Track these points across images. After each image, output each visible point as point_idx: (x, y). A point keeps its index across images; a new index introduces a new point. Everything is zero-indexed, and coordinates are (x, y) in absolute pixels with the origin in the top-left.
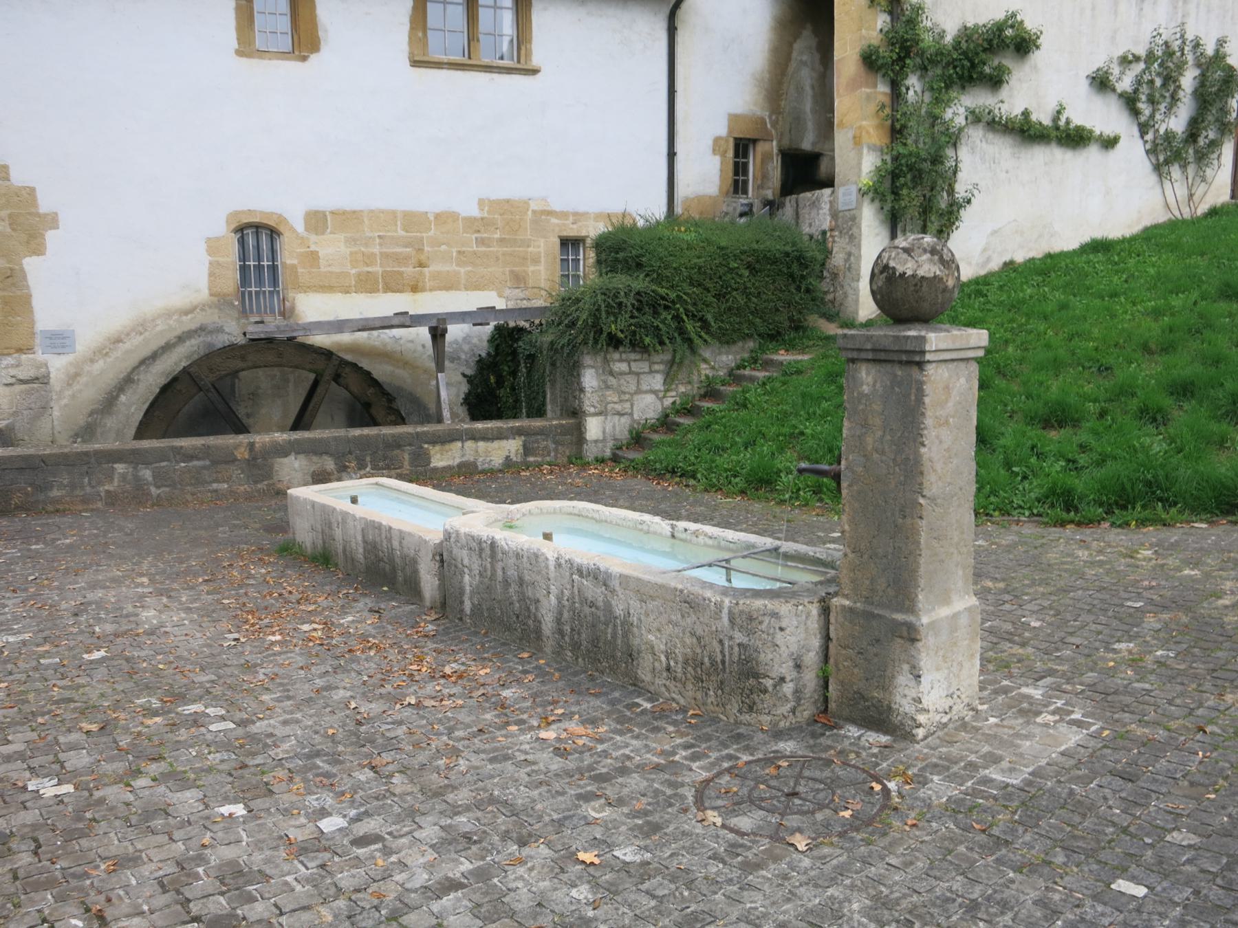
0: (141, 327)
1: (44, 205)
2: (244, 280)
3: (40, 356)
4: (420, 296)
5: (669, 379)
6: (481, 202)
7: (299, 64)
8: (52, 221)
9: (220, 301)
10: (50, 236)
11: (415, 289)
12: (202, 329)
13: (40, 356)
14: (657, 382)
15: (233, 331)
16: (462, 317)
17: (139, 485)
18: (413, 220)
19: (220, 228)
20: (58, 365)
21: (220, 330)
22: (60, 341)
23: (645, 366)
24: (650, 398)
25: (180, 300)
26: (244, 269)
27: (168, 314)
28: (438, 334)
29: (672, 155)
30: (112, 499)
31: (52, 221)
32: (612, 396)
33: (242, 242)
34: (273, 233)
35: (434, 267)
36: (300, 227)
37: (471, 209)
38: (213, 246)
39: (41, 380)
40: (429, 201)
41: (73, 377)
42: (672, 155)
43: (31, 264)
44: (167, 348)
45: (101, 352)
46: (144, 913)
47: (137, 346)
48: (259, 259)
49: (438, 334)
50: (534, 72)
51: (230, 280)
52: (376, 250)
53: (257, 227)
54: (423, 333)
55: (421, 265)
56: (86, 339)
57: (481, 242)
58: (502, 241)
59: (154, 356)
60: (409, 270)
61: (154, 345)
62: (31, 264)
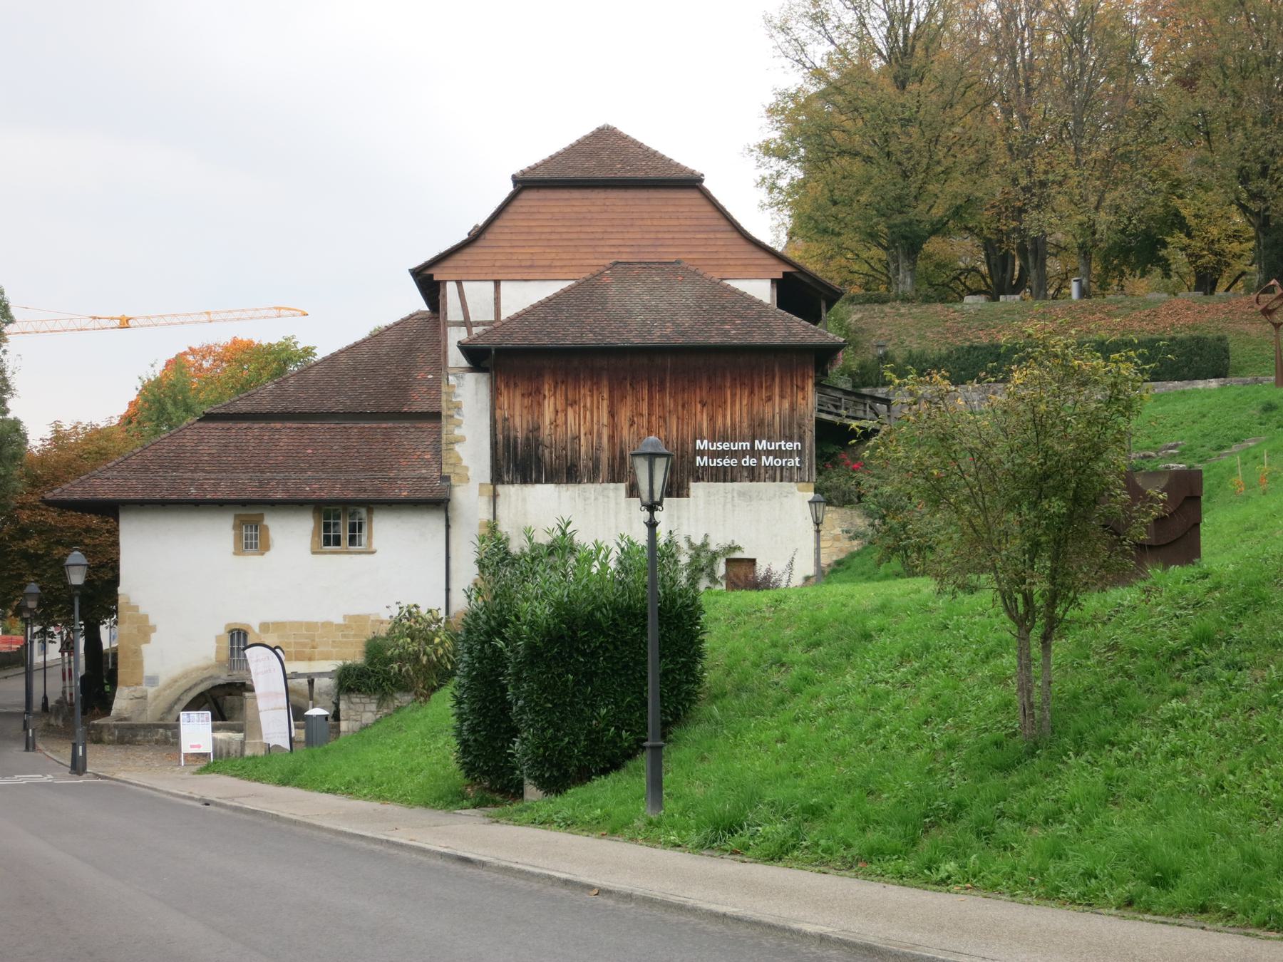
0: (185, 675)
1: (152, 621)
2: (232, 655)
3: (144, 687)
4: (312, 663)
5: (379, 706)
6: (345, 617)
7: (257, 558)
8: (154, 629)
9: (220, 664)
10: (153, 635)
11: (310, 659)
12: (211, 677)
13: (144, 687)
14: (373, 707)
15: (223, 678)
16: (321, 674)
17: (167, 737)
18: (310, 626)
19: (221, 630)
20: (151, 691)
21: (219, 677)
22: (153, 680)
23: (367, 700)
24: (370, 714)
25: (202, 663)
26: (232, 649)
27: (198, 669)
28: (311, 683)
29: (448, 590)
30: (157, 742)
31: (154, 629)
32: (352, 713)
33: (232, 637)
34: (245, 635)
35: (320, 649)
36: (257, 630)
37: (339, 620)
38: (218, 639)
39: (144, 698)
40: (318, 617)
41: (156, 698)
42: (448, 590)
43: (144, 647)
44: (196, 685)
45: (169, 686)
46: (40, 533)
47: (184, 684)
48: (768, 453)
49: (311, 683)
50: (373, 552)
51: (226, 653)
52: (292, 640)
53: (239, 631)
54: (305, 681)
55: (314, 647)
56: (163, 680)
57: (344, 636)
58: (355, 635)
59: (190, 689)
60: (308, 650)
61: (191, 684)
62: (144, 647)
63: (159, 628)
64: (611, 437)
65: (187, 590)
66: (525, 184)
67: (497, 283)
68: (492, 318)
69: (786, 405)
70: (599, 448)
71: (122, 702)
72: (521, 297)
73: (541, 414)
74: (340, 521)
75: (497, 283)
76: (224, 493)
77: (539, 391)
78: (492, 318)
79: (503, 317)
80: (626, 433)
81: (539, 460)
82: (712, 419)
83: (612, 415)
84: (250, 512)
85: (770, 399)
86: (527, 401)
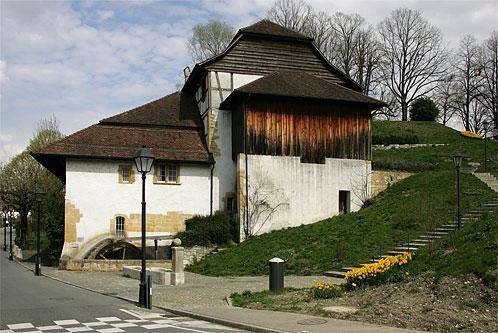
19: (113, 218)
38: (112, 221)
56: (86, 240)
63: (84, 216)
64: (294, 137)
65: (96, 201)
66: (102, 123)
67: (232, 74)
68: (229, 87)
69: (361, 128)
70: (289, 141)
71: (66, 250)
72: (242, 80)
73: (266, 125)
74: (168, 169)
75: (232, 74)
76: (115, 154)
77: (265, 115)
78: (229, 87)
79: (224, 99)
80: (301, 136)
81: (265, 145)
82: (334, 132)
83: (295, 127)
84: (126, 165)
85: (355, 125)
86: (260, 119)
